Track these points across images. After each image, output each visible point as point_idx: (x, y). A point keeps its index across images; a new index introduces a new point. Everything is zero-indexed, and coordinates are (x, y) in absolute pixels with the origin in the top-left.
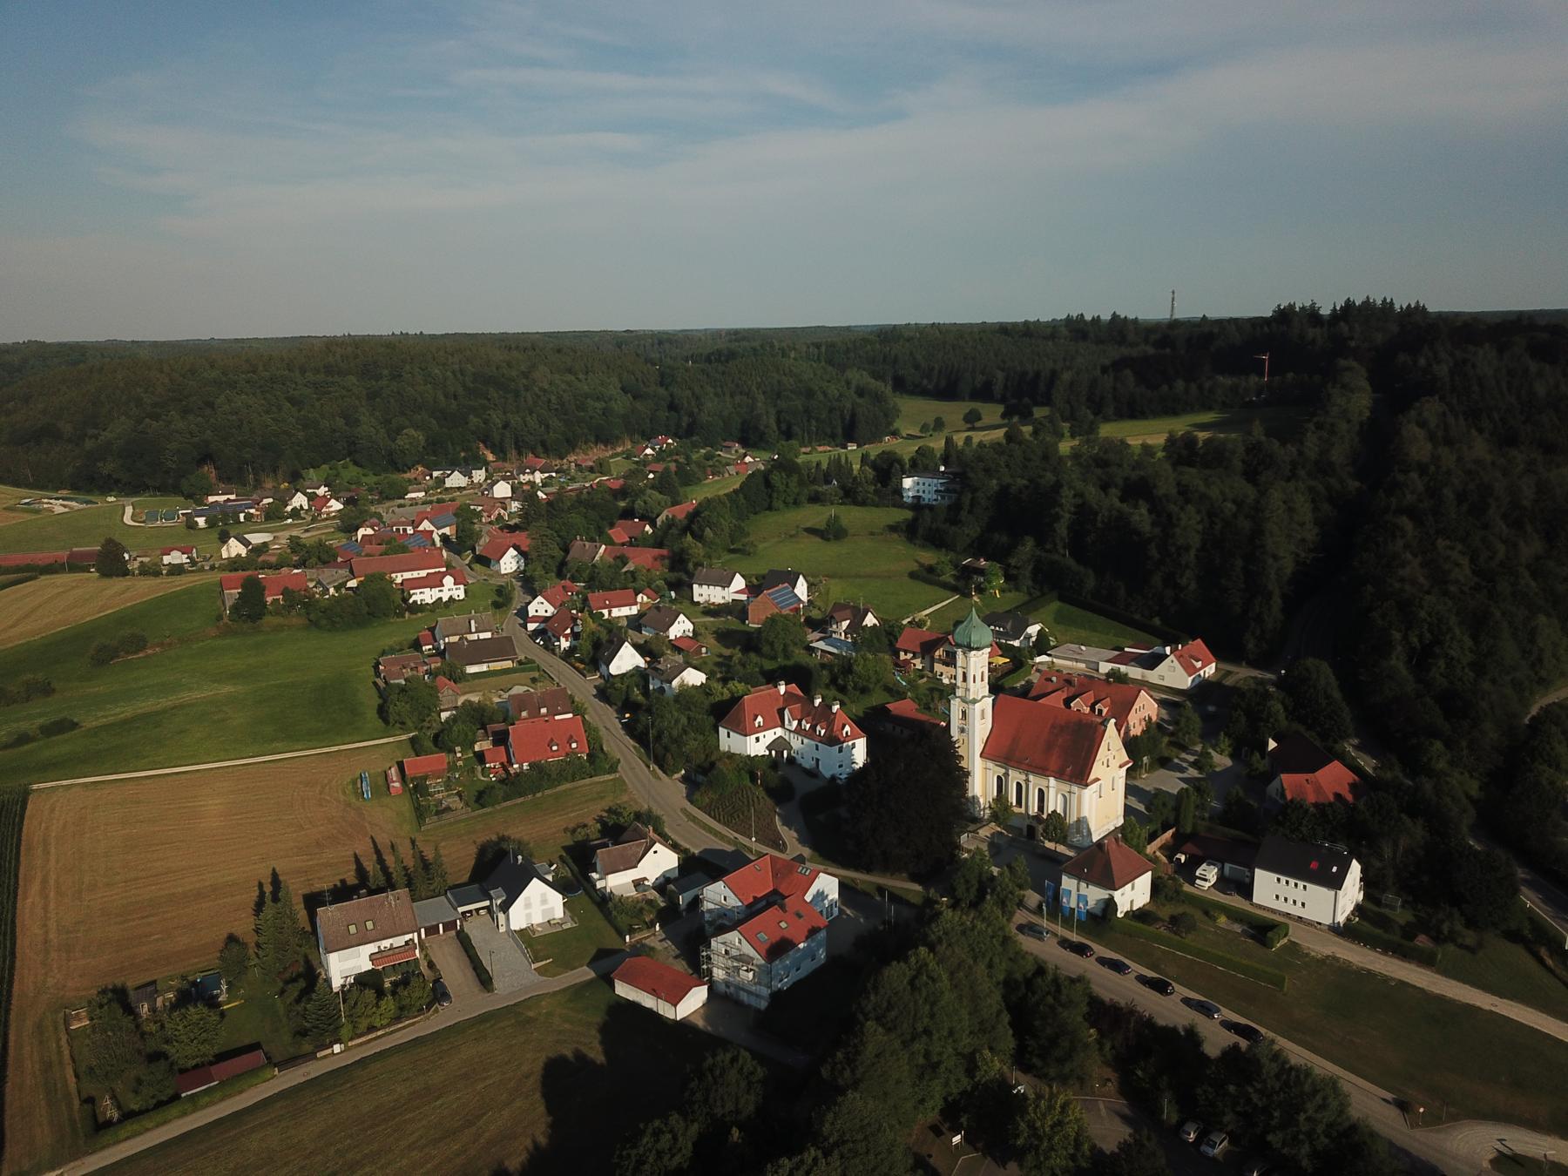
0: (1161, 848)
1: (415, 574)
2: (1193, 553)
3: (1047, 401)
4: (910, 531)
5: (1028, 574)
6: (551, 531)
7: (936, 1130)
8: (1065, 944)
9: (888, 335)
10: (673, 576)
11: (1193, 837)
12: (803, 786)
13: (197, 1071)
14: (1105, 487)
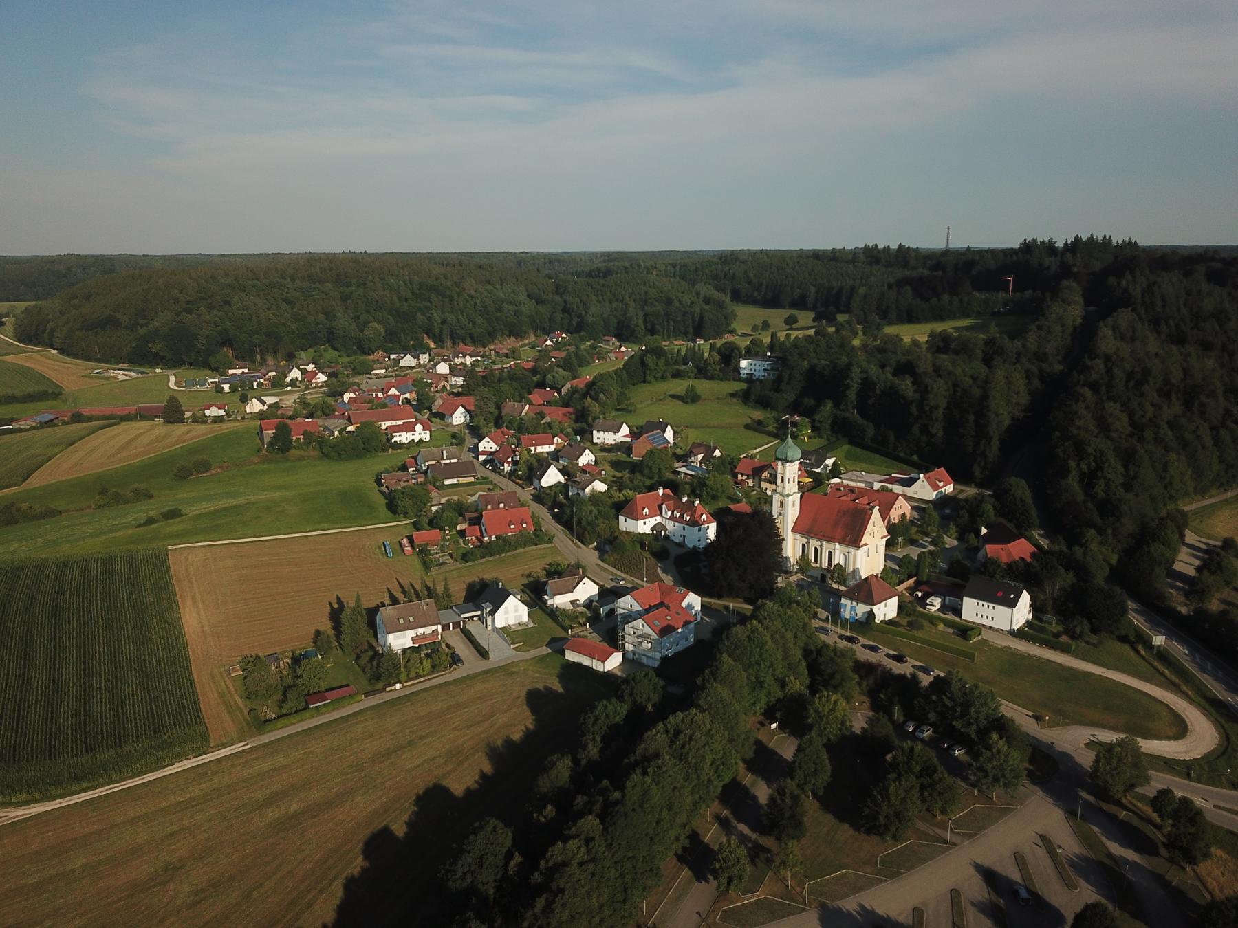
0: (906, 589)
1: (394, 423)
2: (941, 411)
3: (847, 310)
6: (490, 397)
7: (762, 724)
9: (728, 258)
10: (578, 425)
11: (927, 583)
12: (674, 552)
13: (319, 695)
14: (883, 367)
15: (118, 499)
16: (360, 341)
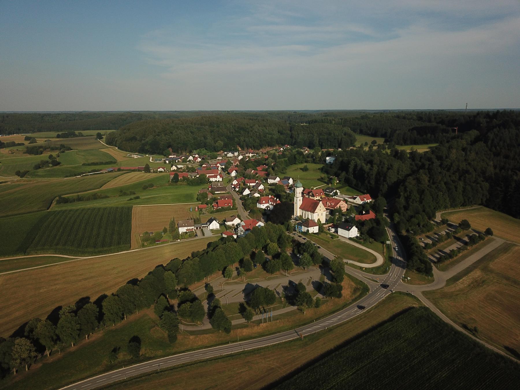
4: (322, 170)
15: (125, 194)
16: (214, 147)
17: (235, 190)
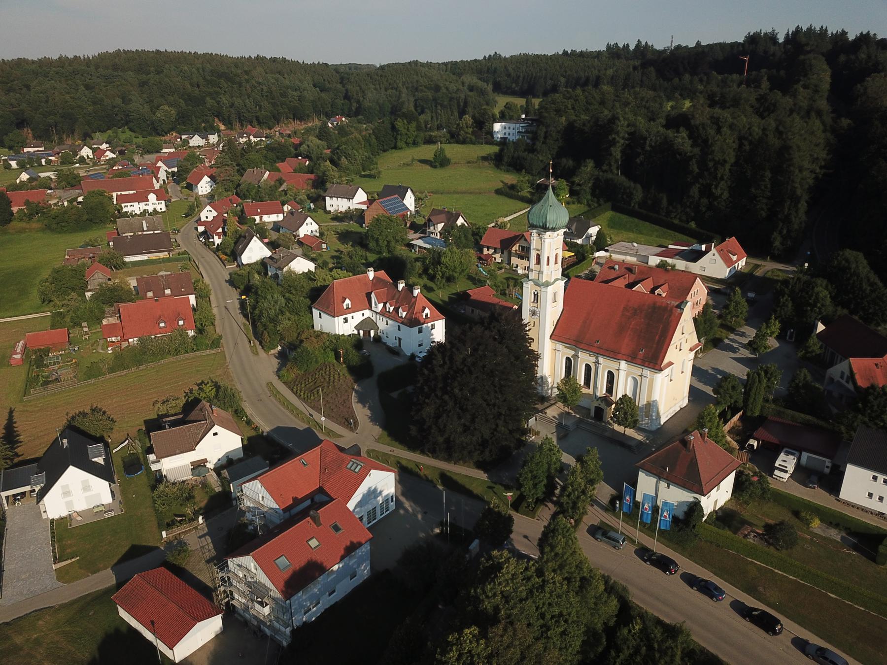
2: (728, 167)
4: (497, 160)
5: (588, 190)
6: (234, 164)
8: (644, 553)
12: (383, 363)
16: (153, 123)
17: (208, 244)
